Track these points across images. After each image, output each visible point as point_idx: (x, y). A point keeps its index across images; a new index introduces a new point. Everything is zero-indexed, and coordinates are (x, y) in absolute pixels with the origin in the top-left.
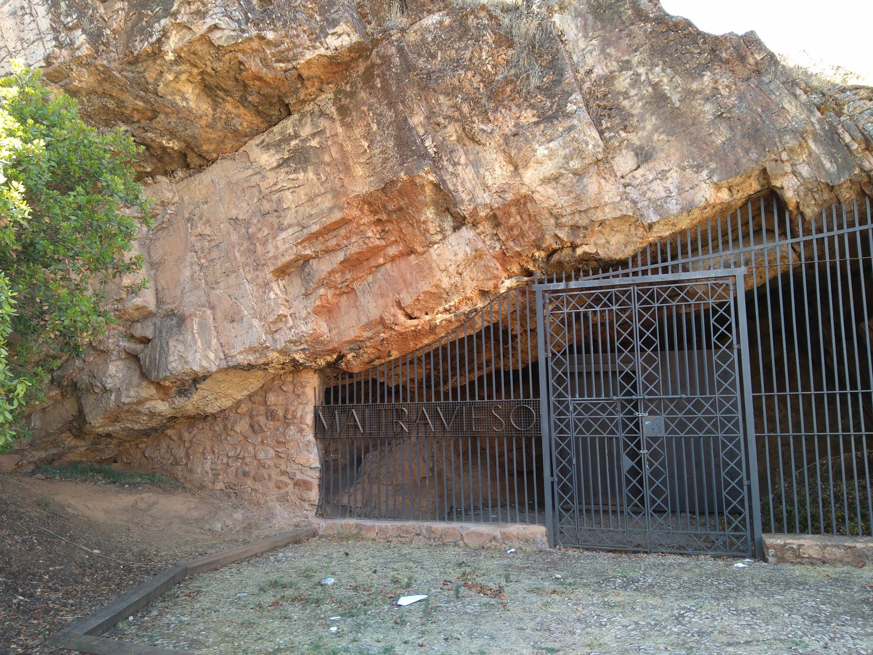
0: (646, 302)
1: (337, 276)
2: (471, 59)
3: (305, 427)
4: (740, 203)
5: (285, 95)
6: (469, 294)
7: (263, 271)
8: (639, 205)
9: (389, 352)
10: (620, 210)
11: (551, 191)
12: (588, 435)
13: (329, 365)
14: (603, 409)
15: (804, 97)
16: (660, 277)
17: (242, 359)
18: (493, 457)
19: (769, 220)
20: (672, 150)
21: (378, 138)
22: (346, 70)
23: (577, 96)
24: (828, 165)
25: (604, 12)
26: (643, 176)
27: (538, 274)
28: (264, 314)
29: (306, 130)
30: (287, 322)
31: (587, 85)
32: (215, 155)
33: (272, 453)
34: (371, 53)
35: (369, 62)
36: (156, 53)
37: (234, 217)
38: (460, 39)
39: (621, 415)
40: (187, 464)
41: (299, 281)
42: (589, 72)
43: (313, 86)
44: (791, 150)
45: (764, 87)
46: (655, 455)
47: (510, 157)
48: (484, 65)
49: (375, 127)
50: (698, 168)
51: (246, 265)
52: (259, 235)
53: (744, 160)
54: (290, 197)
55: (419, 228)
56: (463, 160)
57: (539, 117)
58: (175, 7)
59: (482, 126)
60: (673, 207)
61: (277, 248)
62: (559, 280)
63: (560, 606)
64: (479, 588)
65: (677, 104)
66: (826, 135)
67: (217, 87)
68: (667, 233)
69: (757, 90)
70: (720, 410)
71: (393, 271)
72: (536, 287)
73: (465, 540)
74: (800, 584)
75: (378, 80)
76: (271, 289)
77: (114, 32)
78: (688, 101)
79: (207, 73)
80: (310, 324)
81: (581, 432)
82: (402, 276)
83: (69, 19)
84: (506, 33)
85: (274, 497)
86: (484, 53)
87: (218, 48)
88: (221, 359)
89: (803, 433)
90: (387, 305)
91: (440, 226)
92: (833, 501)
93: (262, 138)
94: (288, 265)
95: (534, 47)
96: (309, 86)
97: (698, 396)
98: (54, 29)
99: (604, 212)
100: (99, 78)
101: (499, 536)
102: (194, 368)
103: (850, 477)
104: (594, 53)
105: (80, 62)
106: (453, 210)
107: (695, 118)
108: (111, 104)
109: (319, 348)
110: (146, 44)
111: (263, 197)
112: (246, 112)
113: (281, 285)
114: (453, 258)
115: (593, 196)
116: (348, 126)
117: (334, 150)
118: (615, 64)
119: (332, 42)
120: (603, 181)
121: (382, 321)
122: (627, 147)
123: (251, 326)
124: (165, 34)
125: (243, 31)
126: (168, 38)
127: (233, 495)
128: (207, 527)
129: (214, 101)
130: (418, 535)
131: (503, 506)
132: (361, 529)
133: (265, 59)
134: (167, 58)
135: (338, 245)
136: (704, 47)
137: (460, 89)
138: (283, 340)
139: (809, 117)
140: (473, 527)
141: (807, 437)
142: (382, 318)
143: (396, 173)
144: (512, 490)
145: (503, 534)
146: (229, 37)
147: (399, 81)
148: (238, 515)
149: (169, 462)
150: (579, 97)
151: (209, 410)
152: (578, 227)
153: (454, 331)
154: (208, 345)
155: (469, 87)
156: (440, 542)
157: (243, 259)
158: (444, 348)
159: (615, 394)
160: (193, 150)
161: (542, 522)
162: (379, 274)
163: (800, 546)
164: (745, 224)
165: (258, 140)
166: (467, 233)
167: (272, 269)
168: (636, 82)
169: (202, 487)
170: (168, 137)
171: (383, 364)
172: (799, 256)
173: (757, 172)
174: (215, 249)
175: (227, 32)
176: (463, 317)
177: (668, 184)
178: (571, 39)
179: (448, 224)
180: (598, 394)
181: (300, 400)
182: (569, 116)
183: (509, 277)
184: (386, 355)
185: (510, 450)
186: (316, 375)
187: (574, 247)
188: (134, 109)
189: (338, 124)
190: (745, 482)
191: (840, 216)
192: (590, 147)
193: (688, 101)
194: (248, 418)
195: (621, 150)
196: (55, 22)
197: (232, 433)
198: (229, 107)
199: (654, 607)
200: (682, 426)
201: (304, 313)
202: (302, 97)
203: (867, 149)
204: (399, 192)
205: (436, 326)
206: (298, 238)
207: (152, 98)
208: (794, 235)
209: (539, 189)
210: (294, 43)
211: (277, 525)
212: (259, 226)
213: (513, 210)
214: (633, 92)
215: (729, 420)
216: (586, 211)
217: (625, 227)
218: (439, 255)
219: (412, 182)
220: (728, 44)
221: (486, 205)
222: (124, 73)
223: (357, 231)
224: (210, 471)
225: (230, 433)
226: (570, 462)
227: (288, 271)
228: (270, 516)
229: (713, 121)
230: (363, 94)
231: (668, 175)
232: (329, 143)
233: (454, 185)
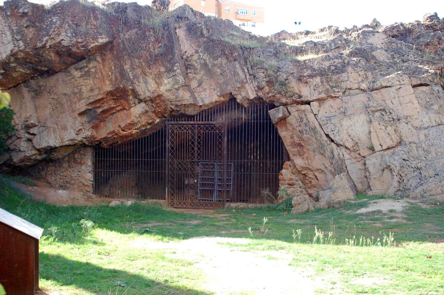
2: (146, 47)
11: (169, 94)
17: (67, 143)
30: (82, 131)
49: (113, 68)
54: (84, 88)
59: (148, 70)
61: (80, 106)
65: (210, 68)
81: (178, 171)
83: (17, 37)
91: (134, 102)
93: (75, 66)
105: (20, 51)
108: (28, 60)
116: (104, 66)
117: (100, 74)
120: (184, 92)
134: (47, 48)
141: (243, 174)
142: (114, 131)
165: (73, 66)
166: (143, 104)
167: (78, 113)
179: (137, 101)
189: (101, 65)
201: (88, 128)
206: (86, 103)
209: (165, 93)
214: (198, 61)
218: (133, 111)
221: (148, 96)
231: (206, 90)
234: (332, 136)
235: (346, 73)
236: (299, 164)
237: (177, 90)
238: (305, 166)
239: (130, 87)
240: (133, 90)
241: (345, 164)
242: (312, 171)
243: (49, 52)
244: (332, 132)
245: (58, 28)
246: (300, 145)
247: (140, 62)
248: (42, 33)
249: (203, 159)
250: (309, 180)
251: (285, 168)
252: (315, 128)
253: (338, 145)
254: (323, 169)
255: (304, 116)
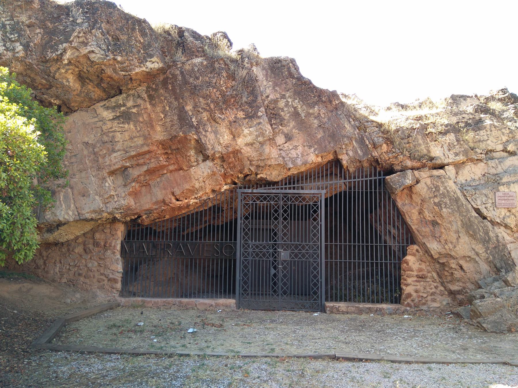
0: (285, 201)
1: (142, 177)
2: (215, 83)
3: (116, 251)
4: (325, 163)
5: (121, 86)
6: (207, 191)
7: (102, 171)
8: (286, 159)
9: (165, 216)
10: (278, 161)
11: (249, 149)
12: (257, 259)
13: (131, 220)
14: (264, 247)
15: (353, 123)
16: (292, 191)
18: (204, 268)
19: (336, 170)
20: (300, 138)
21: (169, 114)
22: (154, 78)
23: (262, 109)
24: (360, 152)
25: (276, 70)
26: (288, 146)
27: (239, 184)
28: (102, 193)
29: (130, 104)
30: (114, 198)
31: (266, 102)
32: (76, 108)
33: (96, 264)
34: (166, 71)
35: (165, 76)
36: (59, 58)
37: (86, 142)
38: (211, 73)
39: (272, 250)
40: (44, 268)
41: (121, 178)
42: (268, 97)
43: (136, 83)
44: (346, 145)
45: (338, 116)
46: (285, 268)
47: (232, 131)
48: (222, 87)
49: (168, 108)
50: (310, 147)
51: (92, 167)
52: (101, 153)
53: (328, 146)
54: (120, 136)
55: (186, 158)
56: (210, 130)
57: (246, 115)
58: (71, 39)
59: (219, 115)
60: (299, 162)
61: (111, 160)
62: (249, 188)
63: (247, 330)
64: (212, 325)
65: (304, 118)
66: (360, 140)
67: (87, 78)
68: (296, 172)
69: (335, 117)
70: (312, 249)
71: (171, 177)
72: (238, 190)
73: (198, 307)
74: (338, 321)
75: (170, 86)
76: (106, 181)
77: (35, 44)
78: (308, 117)
79: (83, 71)
80: (126, 200)
82: (175, 180)
83: (12, 36)
84: (232, 73)
85: (96, 287)
86: (222, 81)
87: (93, 62)
88: (76, 215)
89: (343, 260)
90: (167, 194)
91: (196, 159)
92: (352, 288)
93: (104, 103)
94: (116, 170)
95: (244, 82)
96: (134, 83)
97: (304, 243)
98: (3, 40)
99: (271, 161)
100: (26, 68)
101: (214, 304)
102: (60, 219)
103: (359, 279)
104: (270, 88)
105: (17, 59)
106: (204, 152)
107: (310, 125)
109: (129, 212)
110: (54, 55)
111: (103, 134)
112: (98, 90)
113: (111, 179)
114: (202, 174)
115: (267, 154)
116: (153, 105)
117: (145, 116)
118: (279, 95)
119: (149, 65)
120: (271, 148)
121: (164, 201)
122: (282, 133)
123: (94, 199)
124: (65, 50)
125: (107, 56)
126: (66, 53)
127: (72, 286)
128: (63, 301)
129: (83, 83)
130: (174, 305)
131: (208, 292)
132: (144, 302)
133: (115, 69)
134: (64, 62)
135: (144, 162)
136: (316, 94)
137: (210, 97)
138: (111, 207)
139: (354, 132)
140: (201, 300)
142: (164, 200)
143: (178, 132)
144: (212, 285)
145: (216, 303)
146: (99, 58)
147: (181, 88)
148: (78, 295)
149: (34, 267)
150: (264, 110)
151: (61, 240)
152: (260, 166)
153: (197, 208)
154: (68, 207)
155: (214, 96)
156: (186, 308)
157: (91, 164)
158: (193, 214)
159: (270, 241)
160: (66, 105)
161: (234, 298)
162: (163, 178)
163: (339, 306)
164: (327, 170)
165: (102, 103)
166: (209, 163)
167: (107, 171)
168: (287, 105)
169: (54, 281)
170: (55, 98)
171: (160, 221)
172: (346, 187)
173: (333, 152)
174: (74, 157)
175: (99, 55)
176: (203, 201)
177: (297, 151)
178: (260, 79)
179: (201, 158)
180: (263, 241)
181: (113, 237)
182: (259, 117)
183: (226, 184)
184: (163, 217)
185: (213, 264)
186: (123, 225)
187: (257, 174)
188: (40, 84)
189: (148, 103)
190: (320, 280)
191: (362, 172)
192: (267, 132)
193: (308, 117)
194: (82, 245)
195: (279, 134)
196: (3, 36)
197: (73, 253)
198: (90, 87)
199: (285, 329)
200: (296, 256)
201: (123, 195)
202: (129, 87)
203: (374, 147)
204: (179, 141)
205: (190, 205)
206: (123, 157)
207: (51, 79)
208: (345, 179)
209: (244, 148)
210: (130, 63)
211: (99, 301)
212: (101, 148)
213: (231, 155)
214: (285, 109)
215: (315, 254)
216: (263, 160)
217: (279, 168)
218: (195, 172)
219: (185, 138)
220: (326, 94)
221: (219, 152)
222: (39, 66)
223: (155, 157)
224: (58, 273)
225: (71, 253)
226: (248, 271)
227: (116, 173)
228: (95, 296)
229: (317, 128)
230: (161, 91)
232: (143, 112)
233: (205, 141)
234: (485, 212)
235: (484, 131)
236: (436, 248)
237: (262, 144)
238: (443, 251)
239: (195, 137)
240: (198, 141)
241: (507, 249)
242: (454, 259)
243: (66, 72)
244: (484, 206)
245: (84, 33)
246: (434, 223)
247: (207, 104)
248: (56, 38)
249: (291, 241)
250: (450, 272)
251: (410, 255)
252: (457, 200)
253: (493, 223)
254: (472, 257)
255: (440, 184)
